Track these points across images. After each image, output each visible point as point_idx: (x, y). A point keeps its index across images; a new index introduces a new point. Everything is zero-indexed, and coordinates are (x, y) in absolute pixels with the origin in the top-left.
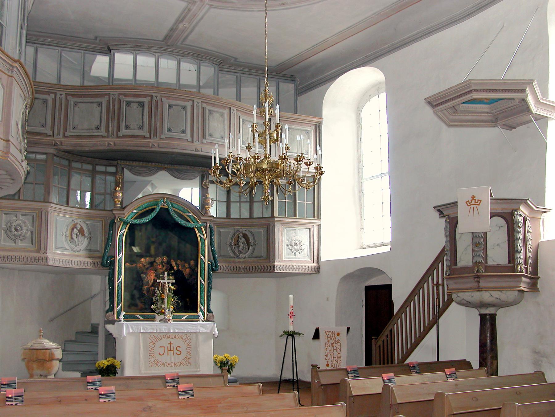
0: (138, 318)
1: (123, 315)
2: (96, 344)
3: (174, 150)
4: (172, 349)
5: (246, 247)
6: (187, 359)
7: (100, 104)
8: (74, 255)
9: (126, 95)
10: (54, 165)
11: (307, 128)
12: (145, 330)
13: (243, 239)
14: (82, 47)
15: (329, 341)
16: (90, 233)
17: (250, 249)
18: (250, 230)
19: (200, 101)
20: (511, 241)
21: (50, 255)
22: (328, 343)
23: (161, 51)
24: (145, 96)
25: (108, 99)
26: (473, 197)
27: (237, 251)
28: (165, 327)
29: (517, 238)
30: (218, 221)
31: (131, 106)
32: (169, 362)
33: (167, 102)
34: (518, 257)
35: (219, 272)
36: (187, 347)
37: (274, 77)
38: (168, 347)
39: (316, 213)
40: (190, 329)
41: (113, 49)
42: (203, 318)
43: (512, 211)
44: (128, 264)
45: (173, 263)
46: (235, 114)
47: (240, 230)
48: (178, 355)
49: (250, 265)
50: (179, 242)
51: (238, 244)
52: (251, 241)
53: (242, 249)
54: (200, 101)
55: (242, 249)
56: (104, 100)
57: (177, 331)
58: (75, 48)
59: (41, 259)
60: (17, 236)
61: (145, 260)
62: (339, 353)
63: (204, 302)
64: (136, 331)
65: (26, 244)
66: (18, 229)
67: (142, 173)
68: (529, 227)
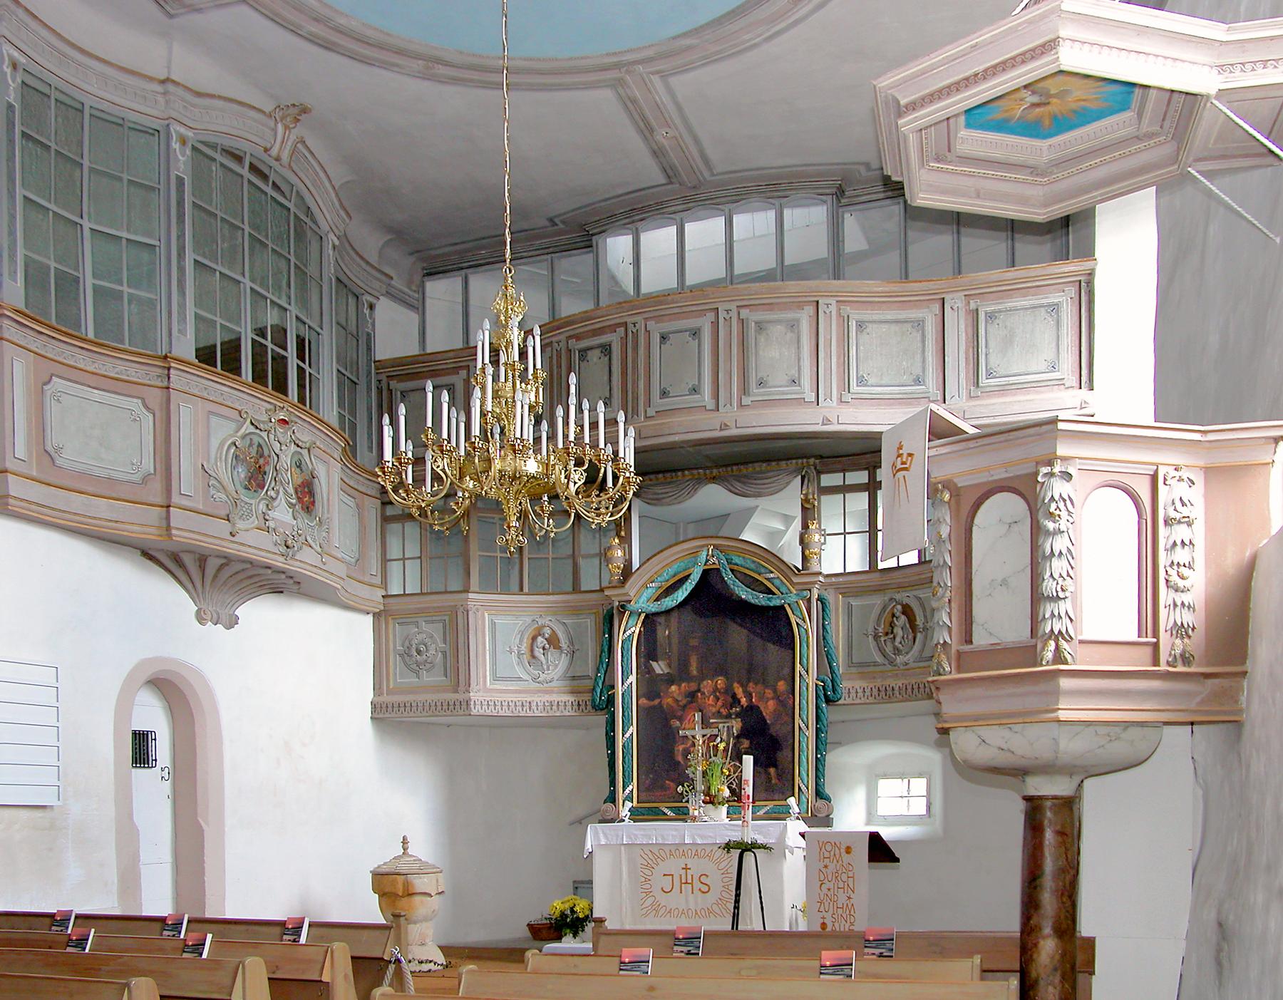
2: (589, 886)
3: (676, 438)
9: (578, 337)
11: (1054, 298)
12: (631, 838)
13: (903, 618)
15: (826, 867)
16: (572, 643)
19: (733, 306)
21: (481, 694)
22: (824, 870)
24: (613, 328)
27: (892, 649)
28: (674, 833)
31: (589, 358)
33: (656, 329)
35: (845, 702)
42: (798, 811)
44: (643, 701)
45: (739, 691)
46: (834, 313)
47: (898, 597)
48: (703, 892)
50: (749, 643)
51: (892, 632)
52: (920, 621)
53: (901, 643)
54: (733, 306)
55: (901, 643)
57: (699, 841)
61: (679, 689)
63: (808, 775)
64: (614, 842)
67: (664, 498)
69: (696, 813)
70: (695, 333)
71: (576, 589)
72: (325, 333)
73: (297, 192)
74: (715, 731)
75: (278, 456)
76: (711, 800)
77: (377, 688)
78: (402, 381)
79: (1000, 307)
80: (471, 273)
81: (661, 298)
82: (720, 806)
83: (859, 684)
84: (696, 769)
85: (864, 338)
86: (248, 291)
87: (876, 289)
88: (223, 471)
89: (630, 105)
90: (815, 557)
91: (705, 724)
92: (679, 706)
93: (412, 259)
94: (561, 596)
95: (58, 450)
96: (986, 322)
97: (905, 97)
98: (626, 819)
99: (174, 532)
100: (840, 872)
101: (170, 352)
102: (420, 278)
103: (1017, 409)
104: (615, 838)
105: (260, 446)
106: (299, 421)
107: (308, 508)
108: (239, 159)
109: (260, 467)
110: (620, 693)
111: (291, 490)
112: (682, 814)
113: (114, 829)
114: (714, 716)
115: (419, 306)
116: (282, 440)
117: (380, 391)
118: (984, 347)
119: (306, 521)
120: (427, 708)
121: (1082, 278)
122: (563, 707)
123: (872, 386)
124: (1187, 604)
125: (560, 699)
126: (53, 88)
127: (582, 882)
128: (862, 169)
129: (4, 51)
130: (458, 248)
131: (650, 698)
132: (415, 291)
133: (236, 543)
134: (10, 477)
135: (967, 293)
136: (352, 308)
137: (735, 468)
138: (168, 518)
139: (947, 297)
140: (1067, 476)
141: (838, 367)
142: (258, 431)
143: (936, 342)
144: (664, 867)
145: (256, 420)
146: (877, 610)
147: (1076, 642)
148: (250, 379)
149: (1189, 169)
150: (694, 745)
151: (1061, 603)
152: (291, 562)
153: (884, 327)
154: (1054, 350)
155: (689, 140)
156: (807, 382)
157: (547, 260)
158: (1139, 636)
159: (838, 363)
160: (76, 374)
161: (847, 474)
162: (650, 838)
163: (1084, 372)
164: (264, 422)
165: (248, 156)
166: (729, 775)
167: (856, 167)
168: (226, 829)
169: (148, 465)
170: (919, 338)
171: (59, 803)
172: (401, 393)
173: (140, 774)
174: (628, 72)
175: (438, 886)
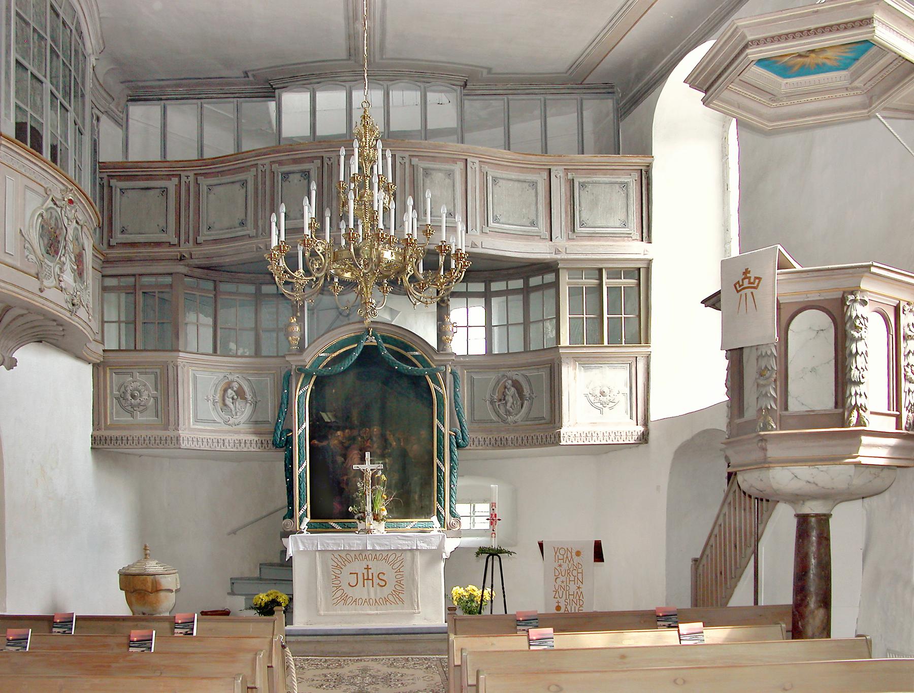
0: (333, 527)
1: (306, 523)
4: (370, 578)
5: (519, 403)
6: (396, 593)
7: (244, 183)
8: (229, 432)
9: (280, 163)
10: (186, 291)
12: (323, 546)
13: (513, 389)
14: (233, 93)
15: (560, 566)
16: (255, 395)
17: (525, 406)
18: (522, 372)
19: (406, 155)
20: (840, 361)
21: (186, 432)
22: (558, 568)
23: (355, 78)
24: (311, 159)
25: (255, 174)
26: (746, 272)
27: (504, 411)
29: (851, 352)
30: (468, 362)
31: (290, 179)
32: (366, 597)
34: (853, 393)
35: (470, 448)
36: (339, 576)
37: (573, 91)
38: (363, 574)
39: (641, 336)
40: (401, 544)
41: (278, 88)
43: (843, 296)
46: (477, 169)
47: (509, 374)
48: (383, 586)
49: (474, 437)
51: (504, 400)
52: (526, 392)
54: (406, 155)
55: (511, 407)
56: (249, 176)
57: (378, 548)
59: (170, 439)
61: (344, 435)
62: (579, 588)
64: (310, 548)
68: (908, 325)
77: (96, 424)
78: (120, 180)
79: (589, 180)
80: (169, 105)
81: (293, 145)
83: (480, 436)
85: (497, 188)
87: (506, 156)
88: (34, 236)
93: (123, 86)
94: (248, 359)
96: (579, 189)
97: (751, 35)
98: (305, 531)
100: (571, 569)
103: (601, 250)
104: (311, 545)
115: (123, 123)
116: (70, 216)
117: (102, 186)
118: (578, 206)
120: (142, 441)
121: (643, 168)
122: (249, 445)
123: (503, 224)
124: (859, 393)
125: (246, 438)
127: (237, 579)
128: (485, 72)
130: (162, 83)
132: (120, 112)
133: (42, 297)
135: (566, 167)
139: (553, 169)
140: (864, 303)
141: (480, 208)
142: (55, 207)
143: (545, 198)
144: (350, 568)
146: (492, 384)
147: (868, 412)
149: (877, 114)
151: (861, 386)
152: (73, 317)
153: (511, 184)
154: (626, 214)
157: (233, 102)
158: (889, 410)
159: (480, 206)
161: (469, 284)
162: (339, 546)
163: (645, 230)
164: (59, 200)
166: (387, 499)
167: (482, 69)
168: (6, 539)
170: (534, 194)
172: (121, 190)
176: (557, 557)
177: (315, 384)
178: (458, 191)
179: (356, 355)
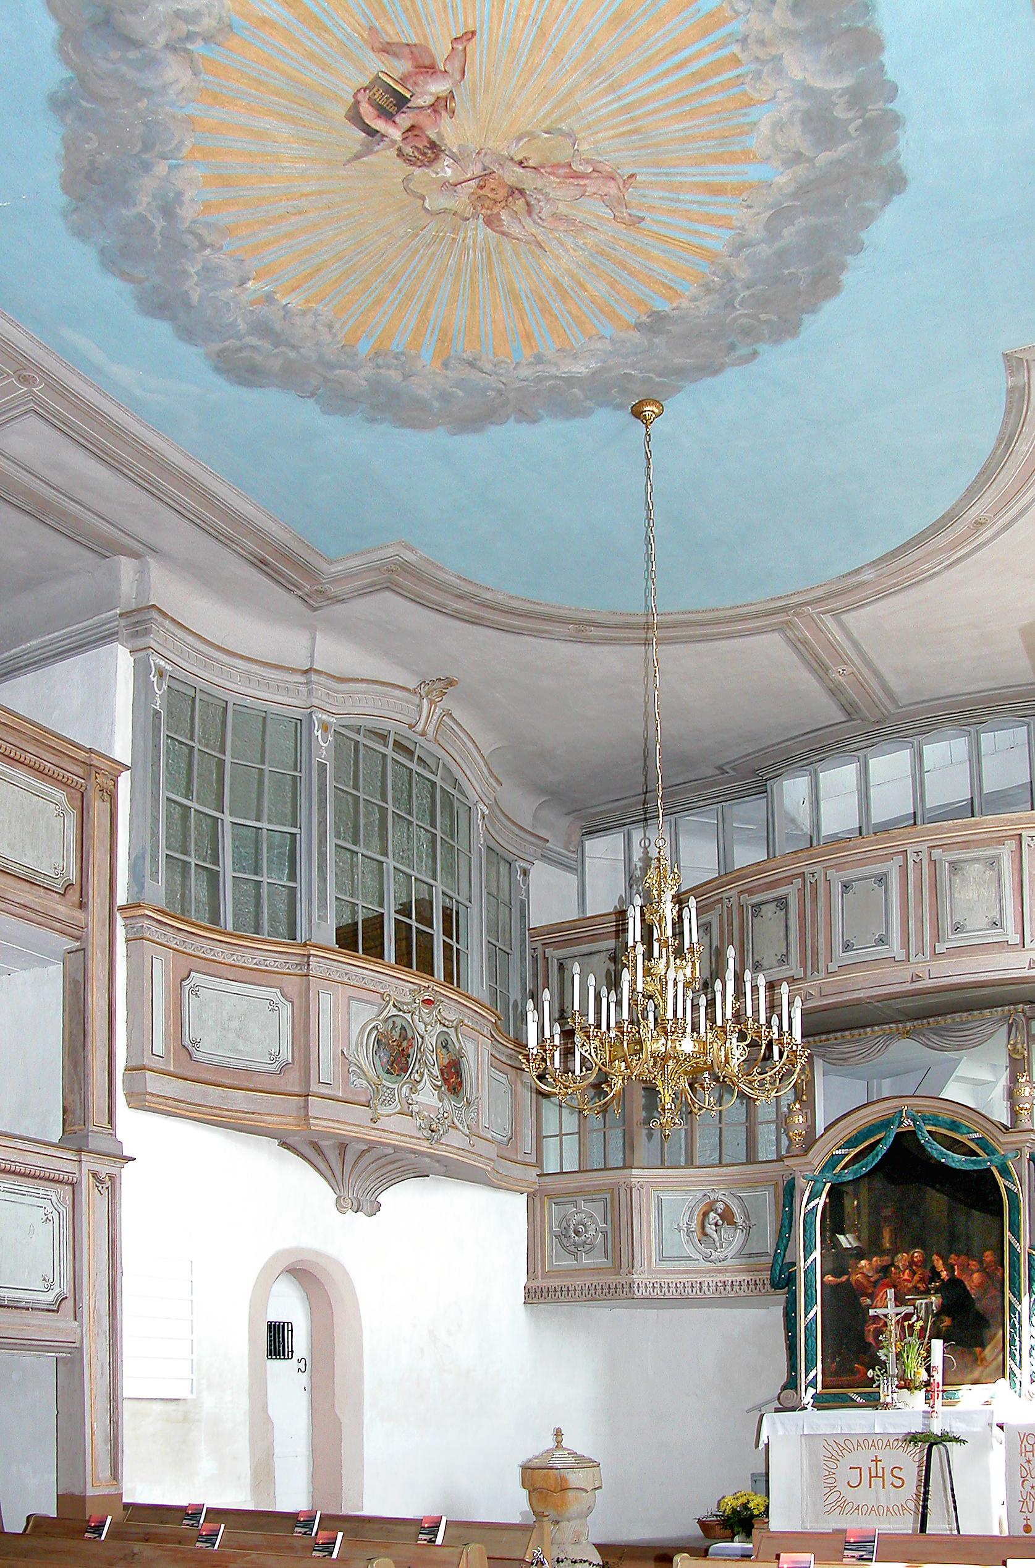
3: (856, 995)
8: (710, 1271)
9: (750, 892)
15: (1028, 1461)
16: (747, 1217)
19: (924, 847)
22: (1026, 1465)
24: (788, 880)
38: (870, 1468)
44: (829, 1278)
45: (939, 1264)
50: (951, 1211)
58: (701, 803)
60: (579, 1245)
65: (595, 1260)
66: (580, 1230)
69: (889, 1400)
70: (882, 879)
71: (751, 1158)
72: (474, 909)
73: (444, 765)
74: (911, 1309)
75: (422, 1038)
76: (907, 1385)
77: (531, 1272)
81: (838, 841)
82: (916, 1392)
84: (887, 1354)
86: (392, 868)
88: (364, 1059)
89: (799, 645)
90: (1026, 1113)
91: (900, 1301)
92: (871, 1282)
93: (570, 818)
95: (195, 1043)
98: (809, 1407)
99: (312, 1121)
101: (310, 940)
102: (578, 838)
105: (403, 1028)
106: (446, 1001)
107: (454, 1089)
108: (383, 738)
109: (403, 1050)
110: (802, 1270)
111: (436, 1071)
112: (874, 1402)
113: (248, 1423)
114: (910, 1292)
115: (577, 868)
116: (427, 1020)
117: (535, 959)
119: (453, 1102)
120: (586, 1291)
126: (198, 690)
129: (152, 662)
131: (837, 1273)
132: (573, 852)
133: (378, 1129)
134: (148, 1073)
136: (504, 880)
137: (931, 1020)
138: (306, 1107)
142: (401, 1013)
144: (850, 1459)
145: (399, 1002)
148: (393, 962)
150: (886, 1324)
152: (436, 1146)
155: (865, 671)
156: (1010, 923)
160: (215, 968)
165: (392, 733)
169: (286, 1055)
171: (194, 1396)
173: (276, 1366)
174: (796, 614)
175: (594, 1481)
176: (1023, 1446)
177: (829, 1194)
178: (1007, 885)
179: (883, 1148)
